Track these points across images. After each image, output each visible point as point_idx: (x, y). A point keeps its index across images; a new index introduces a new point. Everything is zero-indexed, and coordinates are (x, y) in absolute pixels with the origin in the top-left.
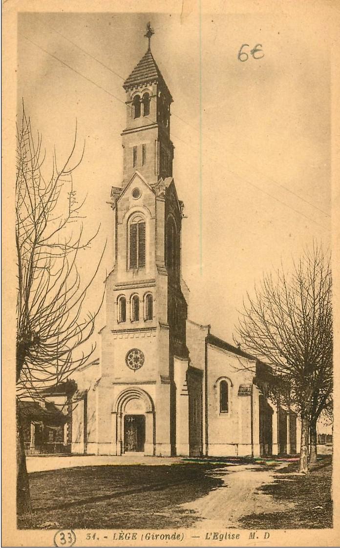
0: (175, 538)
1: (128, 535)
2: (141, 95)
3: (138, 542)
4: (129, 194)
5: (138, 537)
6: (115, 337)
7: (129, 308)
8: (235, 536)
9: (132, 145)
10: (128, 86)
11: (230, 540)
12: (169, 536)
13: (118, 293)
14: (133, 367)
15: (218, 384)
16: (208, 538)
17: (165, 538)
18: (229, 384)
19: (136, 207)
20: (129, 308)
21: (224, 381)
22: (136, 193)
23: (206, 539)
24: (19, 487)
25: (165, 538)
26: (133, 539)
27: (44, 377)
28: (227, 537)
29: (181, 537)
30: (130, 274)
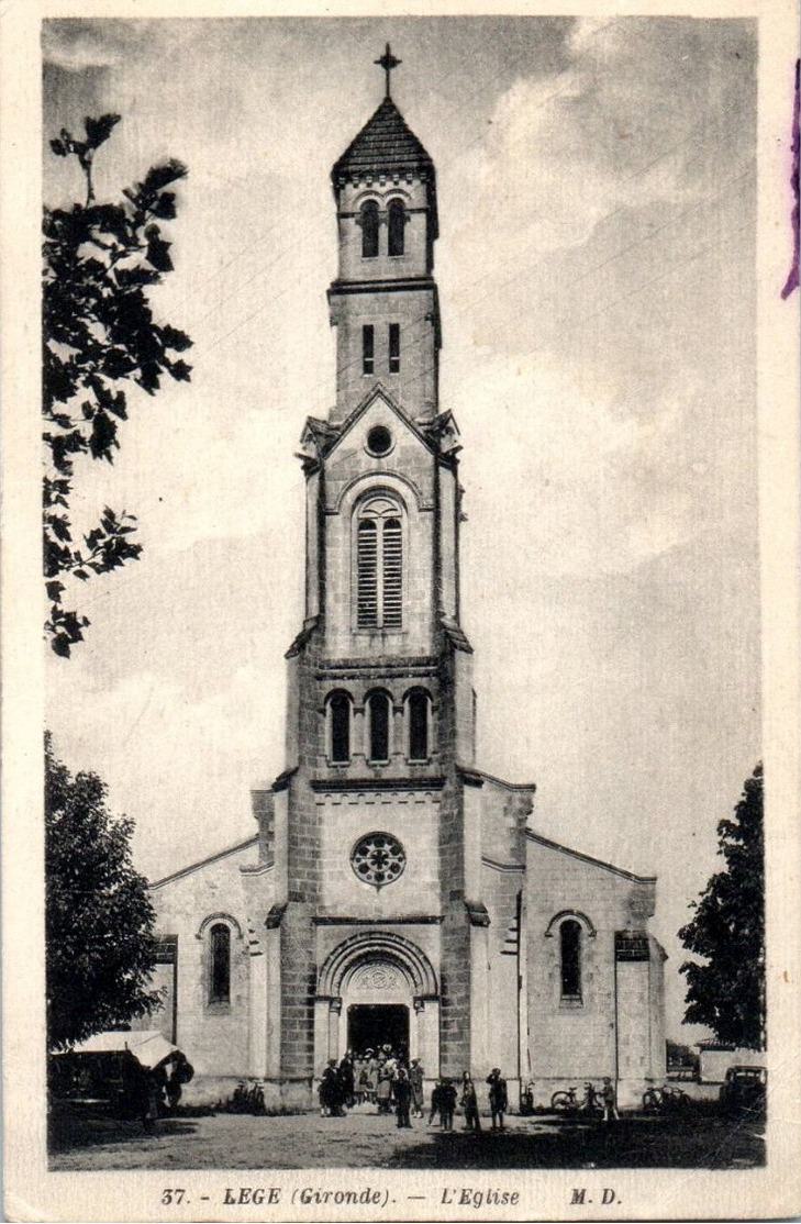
0: (367, 1201)
1: (260, 1194)
2: (383, 204)
3: (288, 1208)
4: (356, 438)
5: (285, 1197)
6: (319, 797)
7: (359, 727)
8: (509, 1198)
9: (357, 323)
10: (342, 174)
11: (497, 1207)
12: (355, 1195)
13: (329, 685)
14: (369, 877)
15: (556, 931)
16: (447, 1200)
17: (346, 1198)
18: (585, 930)
19: (374, 477)
20: (359, 727)
21: (579, 927)
22: (379, 440)
23: (443, 1202)
24: (255, 24)
25: (346, 1198)
26: (270, 1201)
27: (416, 534)
28: (492, 1198)
29: (383, 1199)
30: (363, 640)
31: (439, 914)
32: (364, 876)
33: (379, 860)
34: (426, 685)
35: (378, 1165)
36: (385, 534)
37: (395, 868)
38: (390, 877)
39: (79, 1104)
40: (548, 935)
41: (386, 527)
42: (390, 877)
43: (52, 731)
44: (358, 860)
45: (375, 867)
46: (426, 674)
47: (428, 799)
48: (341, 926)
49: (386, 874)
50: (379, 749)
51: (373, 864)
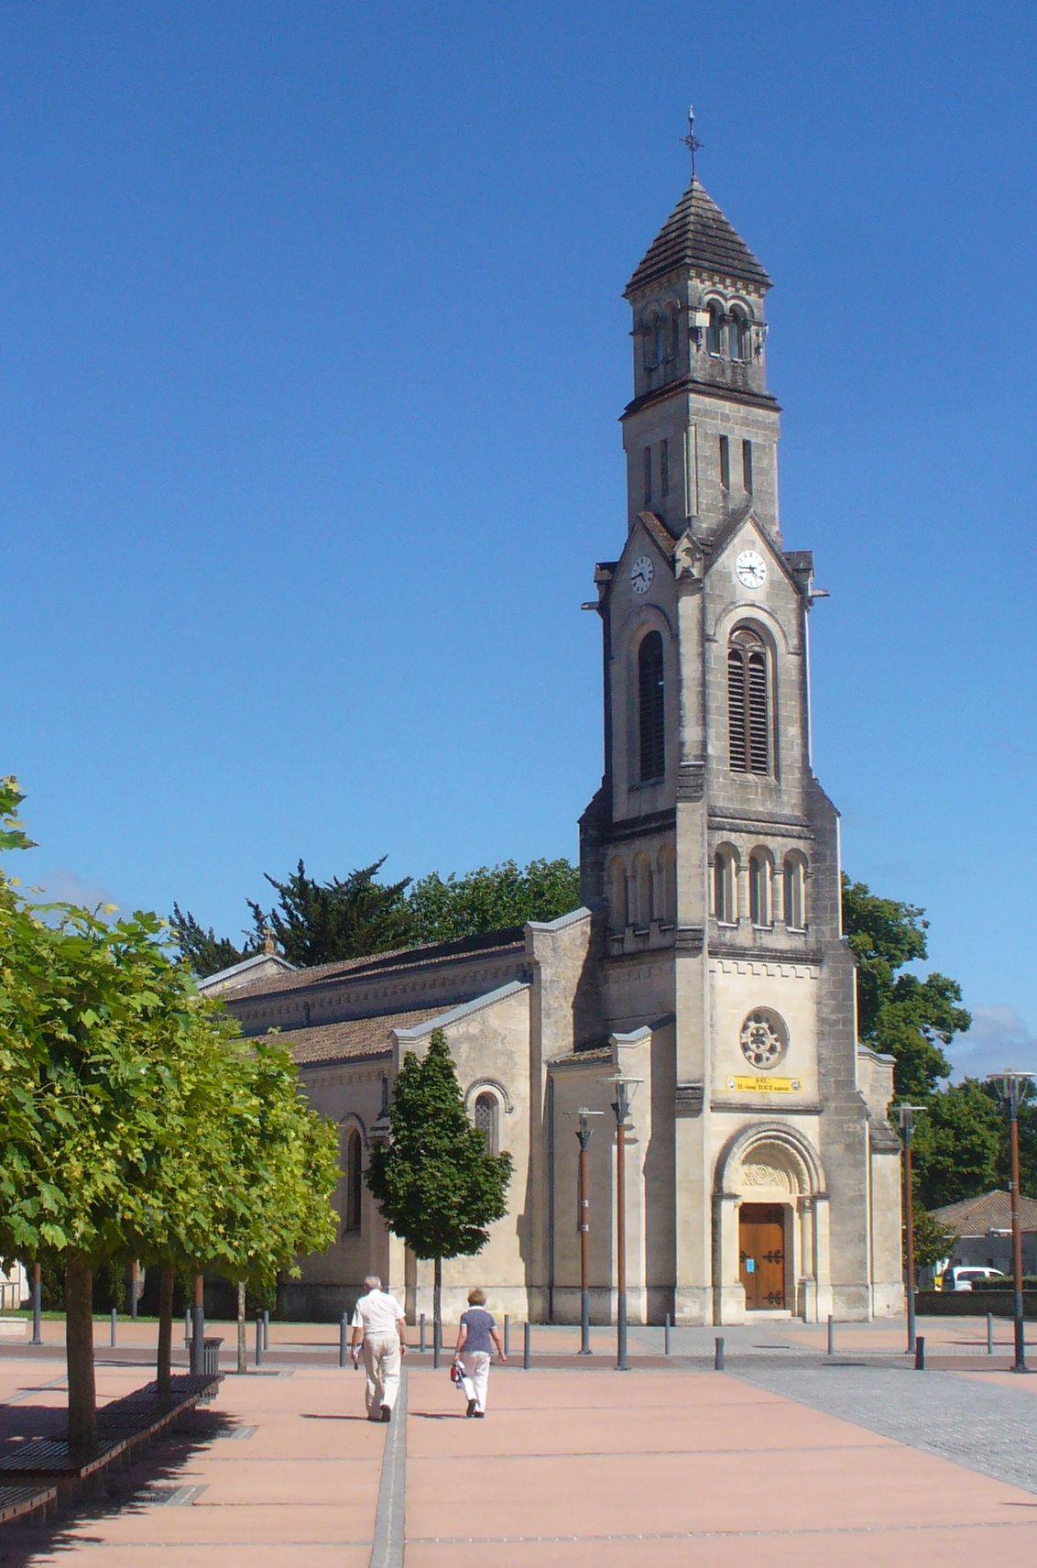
33: (758, 1038)
51: (753, 1042)
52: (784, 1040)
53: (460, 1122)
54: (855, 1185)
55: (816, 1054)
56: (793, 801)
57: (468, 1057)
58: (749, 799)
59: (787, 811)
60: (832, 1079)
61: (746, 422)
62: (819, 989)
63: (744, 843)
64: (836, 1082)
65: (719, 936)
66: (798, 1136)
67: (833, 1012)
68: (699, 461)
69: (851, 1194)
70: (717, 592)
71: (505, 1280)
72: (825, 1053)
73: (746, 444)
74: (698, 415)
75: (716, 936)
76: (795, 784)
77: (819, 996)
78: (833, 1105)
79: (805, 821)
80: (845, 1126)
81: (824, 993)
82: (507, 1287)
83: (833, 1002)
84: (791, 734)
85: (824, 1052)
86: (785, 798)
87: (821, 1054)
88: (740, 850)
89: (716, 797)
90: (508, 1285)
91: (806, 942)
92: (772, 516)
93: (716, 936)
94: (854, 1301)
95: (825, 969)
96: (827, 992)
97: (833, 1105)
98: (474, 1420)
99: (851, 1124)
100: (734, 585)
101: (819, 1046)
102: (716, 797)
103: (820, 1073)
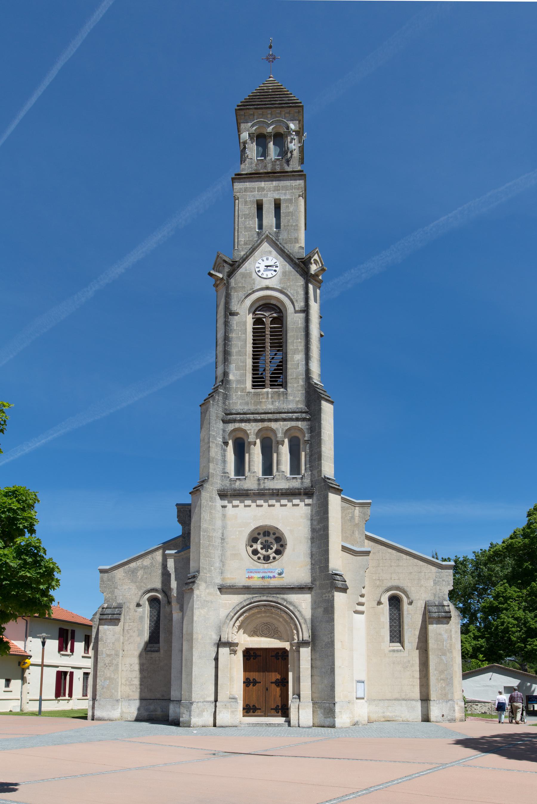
18: (405, 600)
31: (42, 640)
32: (255, 557)
33: (266, 546)
34: (300, 426)
35: (335, 706)
36: (271, 328)
37: (255, 552)
38: (274, 558)
39: (293, 632)
40: (379, 603)
41: (272, 323)
42: (259, 558)
43: (239, 507)
44: (251, 546)
45: (270, 551)
46: (304, 420)
47: (302, 504)
48: (161, 615)
49: (271, 556)
50: (268, 470)
51: (262, 549)
52: (283, 546)
53: (468, 622)
54: (328, 634)
55: (309, 552)
56: (298, 399)
57: (142, 578)
58: (261, 402)
59: (292, 406)
60: (318, 567)
61: (276, 189)
62: (312, 511)
63: (252, 428)
64: (320, 567)
65: (231, 484)
66: (285, 604)
67: (318, 524)
68: (240, 218)
69: (327, 640)
70: (240, 285)
71: (163, 696)
72: (314, 550)
73: (277, 206)
74: (240, 193)
75: (228, 485)
76: (300, 388)
77: (312, 516)
78: (317, 583)
79: (306, 409)
80: (324, 596)
81: (314, 513)
82: (163, 699)
83: (319, 517)
84: (297, 359)
85: (314, 550)
86: (291, 398)
87: (313, 552)
88: (248, 432)
89: (236, 403)
90: (164, 698)
91: (302, 483)
92: (295, 238)
93: (228, 485)
94: (328, 713)
95: (315, 497)
96: (316, 512)
97: (317, 583)
98: (501, 724)
99: (327, 595)
100: (254, 279)
101: (312, 547)
102: (236, 403)
103: (312, 564)
